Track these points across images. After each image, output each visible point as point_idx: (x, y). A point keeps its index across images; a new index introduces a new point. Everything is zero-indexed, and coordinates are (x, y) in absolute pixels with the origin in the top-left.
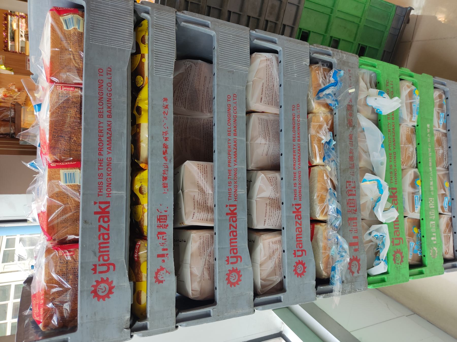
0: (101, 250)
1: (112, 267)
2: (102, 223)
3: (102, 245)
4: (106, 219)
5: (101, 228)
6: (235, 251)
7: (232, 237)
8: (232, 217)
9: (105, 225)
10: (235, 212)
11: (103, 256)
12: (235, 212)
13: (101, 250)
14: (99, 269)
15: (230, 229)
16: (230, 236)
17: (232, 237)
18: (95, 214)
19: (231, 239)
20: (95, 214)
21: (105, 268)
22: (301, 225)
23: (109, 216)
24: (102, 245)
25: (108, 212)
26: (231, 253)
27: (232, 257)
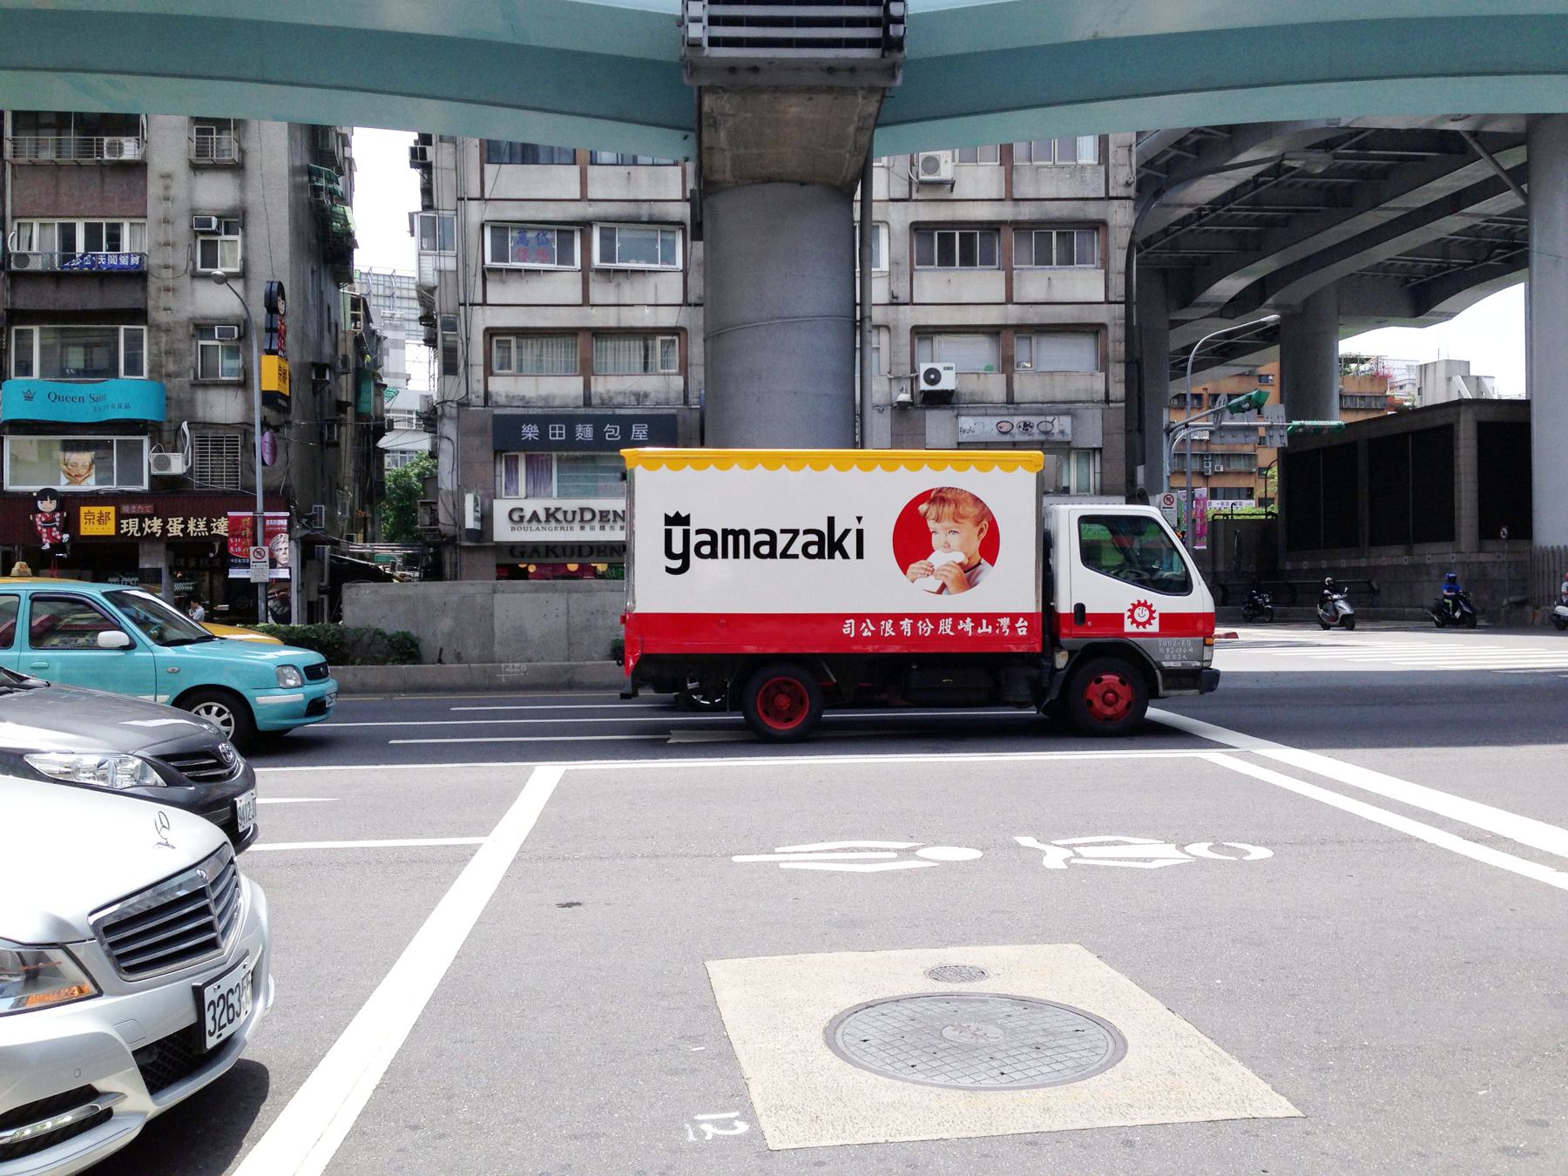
0: (731, 538)
1: (677, 564)
2: (802, 539)
3: (742, 538)
4: (813, 550)
5: (790, 552)
6: (706, 550)
7: (754, 539)
8: (820, 544)
9: (796, 548)
10: (837, 554)
11: (713, 544)
12: (837, 554)
13: (731, 538)
14: (677, 532)
15: (783, 531)
16: (758, 532)
17: (754, 539)
18: (829, 518)
19: (746, 533)
20: (829, 518)
21: (677, 548)
22: (781, 557)
23: (824, 558)
24: (742, 538)
25: (831, 556)
26: (699, 532)
27: (686, 534)
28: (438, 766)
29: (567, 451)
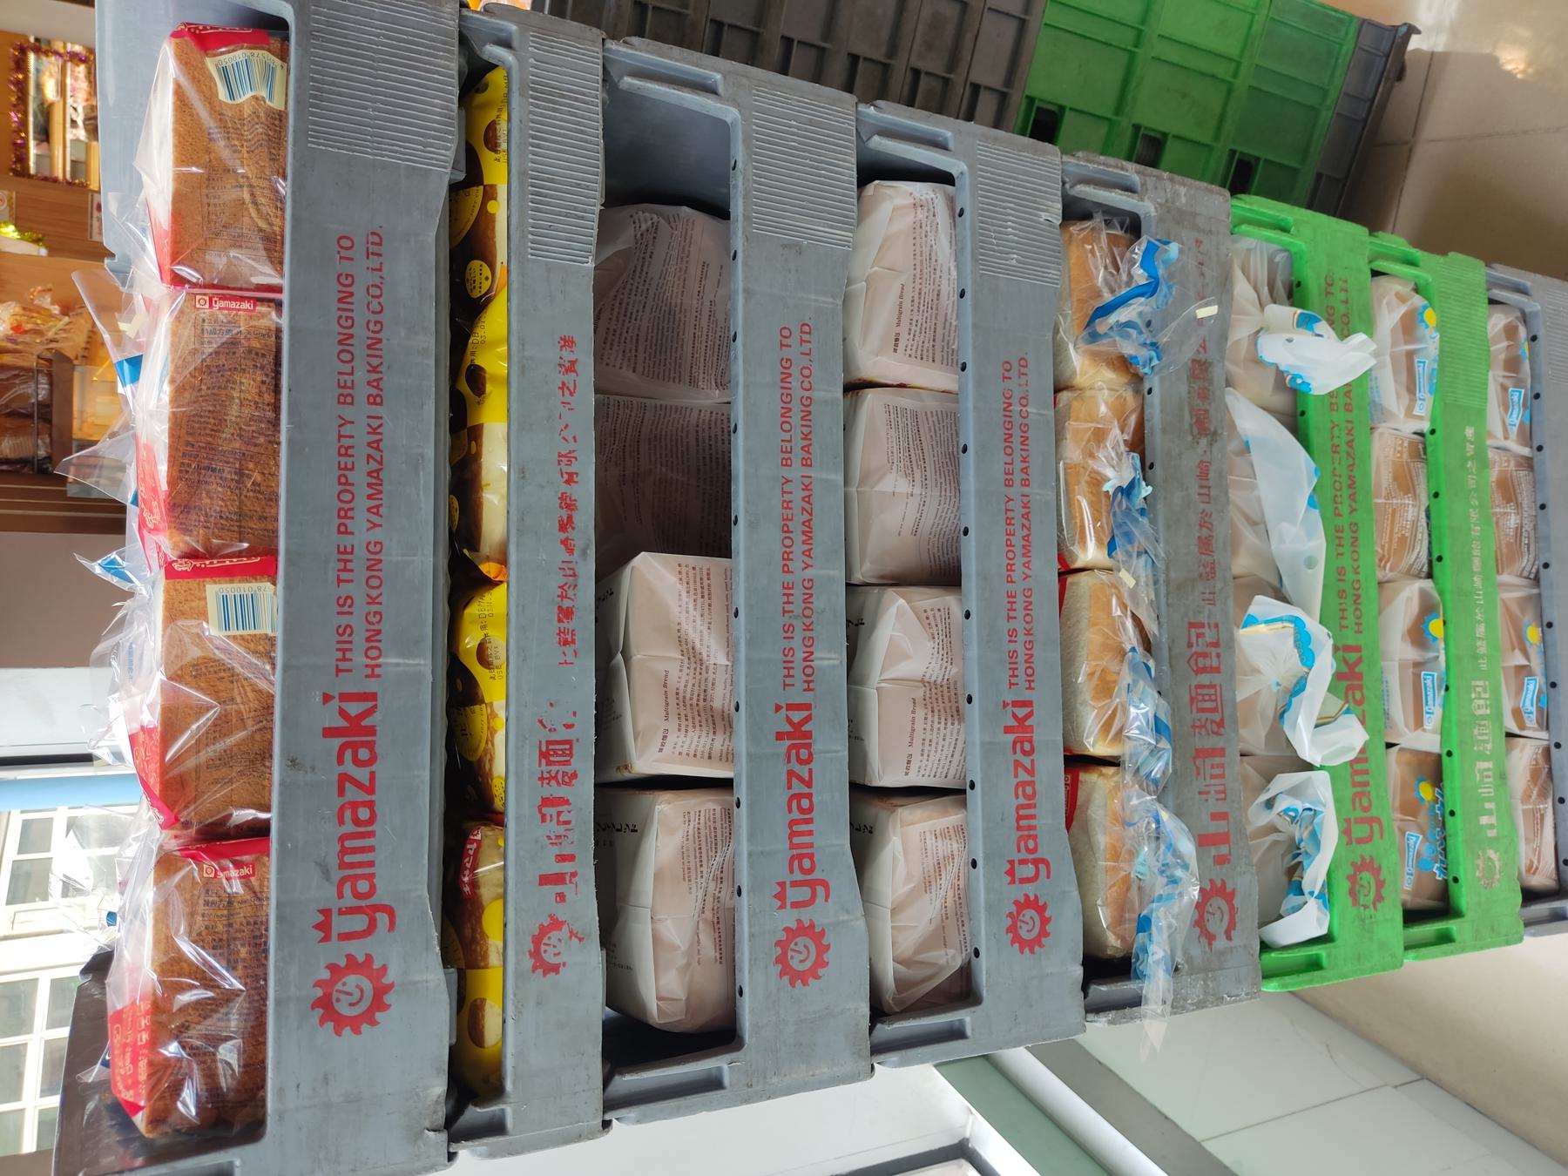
0: (348, 859)
1: (383, 918)
2: (349, 767)
3: (348, 844)
4: (364, 754)
5: (348, 785)
6: (807, 864)
7: (796, 815)
8: (797, 747)
9: (362, 774)
10: (805, 728)
11: (354, 879)
12: (805, 728)
13: (348, 859)
15: (790, 787)
16: (790, 811)
17: (796, 815)
18: (325, 735)
19: (792, 823)
20: (325, 735)
21: (359, 923)
22: (1033, 775)
23: (374, 742)
24: (348, 844)
25: (371, 731)
26: (791, 871)
27: (795, 884)
28: (270, 1074)
29: (1333, 985)
